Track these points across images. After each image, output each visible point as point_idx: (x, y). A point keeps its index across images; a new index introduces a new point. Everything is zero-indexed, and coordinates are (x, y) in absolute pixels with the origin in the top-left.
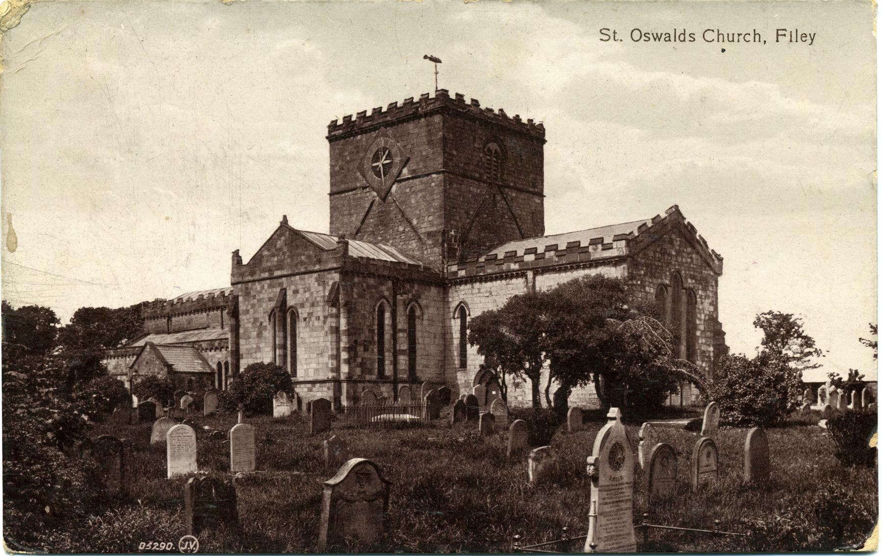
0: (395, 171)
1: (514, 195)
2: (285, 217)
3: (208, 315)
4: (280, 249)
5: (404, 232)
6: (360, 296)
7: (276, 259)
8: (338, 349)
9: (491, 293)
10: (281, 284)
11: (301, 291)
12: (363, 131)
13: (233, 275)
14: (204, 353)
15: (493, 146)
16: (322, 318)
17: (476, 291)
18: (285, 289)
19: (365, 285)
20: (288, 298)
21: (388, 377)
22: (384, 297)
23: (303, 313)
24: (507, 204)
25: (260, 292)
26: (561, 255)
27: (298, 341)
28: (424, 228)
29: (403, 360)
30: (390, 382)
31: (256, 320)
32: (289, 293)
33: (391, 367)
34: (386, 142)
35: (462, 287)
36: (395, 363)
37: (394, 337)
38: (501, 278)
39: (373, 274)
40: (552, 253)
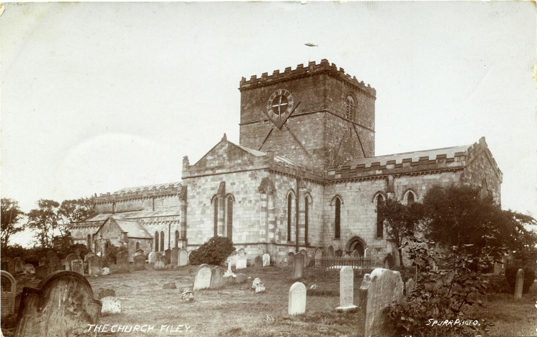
0: (290, 110)
1: (361, 130)
2: (225, 135)
3: (143, 202)
4: (222, 156)
5: (295, 149)
6: (280, 187)
7: (217, 162)
8: (266, 222)
9: (360, 189)
10: (221, 179)
11: (237, 183)
14: (146, 227)
15: (350, 98)
16: (253, 202)
17: (348, 188)
18: (224, 183)
19: (282, 180)
20: (227, 188)
21: (293, 242)
22: (292, 190)
24: (357, 135)
25: (204, 184)
26: (414, 164)
27: (234, 216)
28: (311, 146)
29: (302, 230)
30: (294, 246)
31: (200, 203)
32: (228, 185)
33: (295, 236)
34: (283, 92)
35: (338, 185)
36: (297, 233)
37: (297, 216)
39: (287, 174)
40: (408, 164)
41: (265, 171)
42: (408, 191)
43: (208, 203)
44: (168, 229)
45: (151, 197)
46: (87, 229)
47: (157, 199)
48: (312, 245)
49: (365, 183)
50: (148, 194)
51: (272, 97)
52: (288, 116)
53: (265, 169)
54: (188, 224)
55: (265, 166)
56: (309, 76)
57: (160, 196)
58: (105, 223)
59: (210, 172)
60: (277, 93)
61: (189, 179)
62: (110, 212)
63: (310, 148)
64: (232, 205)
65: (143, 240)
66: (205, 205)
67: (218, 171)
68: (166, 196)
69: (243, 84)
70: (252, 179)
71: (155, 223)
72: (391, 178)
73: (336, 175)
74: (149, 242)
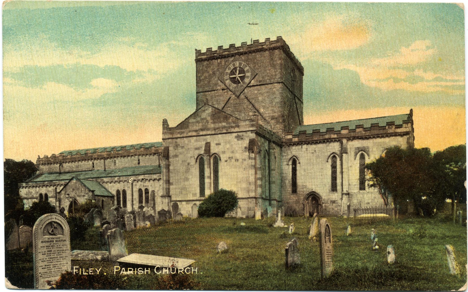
4: (205, 119)
7: (201, 124)
9: (315, 151)
11: (222, 144)
12: (222, 57)
13: (163, 133)
16: (240, 160)
18: (209, 143)
23: (223, 157)
26: (365, 130)
27: (220, 174)
32: (213, 146)
34: (240, 64)
38: (324, 142)
40: (361, 129)
41: (251, 133)
42: (361, 152)
43: (193, 161)
44: (131, 187)
45: (101, 159)
46: (38, 189)
47: (109, 160)
48: (268, 201)
49: (320, 145)
50: (98, 155)
51: (229, 69)
52: (245, 86)
53: (251, 131)
54: (171, 181)
55: (251, 129)
56: (266, 50)
57: (111, 158)
58: (69, 182)
59: (194, 134)
60: (234, 65)
61: (170, 140)
62: (57, 173)
63: (268, 115)
64: (217, 163)
65: (106, 198)
66: (189, 164)
67: (201, 133)
68: (118, 157)
69: (199, 56)
70: (238, 140)
71: (116, 182)
72: (345, 141)
73: (293, 139)
74: (111, 200)
